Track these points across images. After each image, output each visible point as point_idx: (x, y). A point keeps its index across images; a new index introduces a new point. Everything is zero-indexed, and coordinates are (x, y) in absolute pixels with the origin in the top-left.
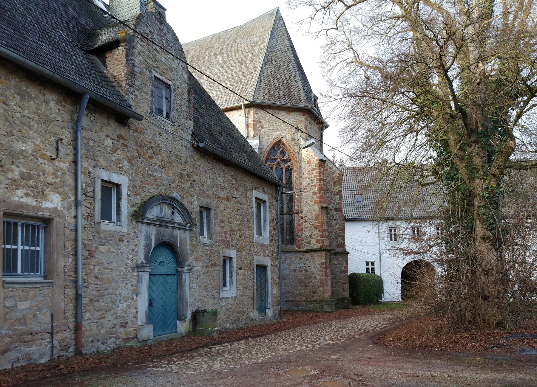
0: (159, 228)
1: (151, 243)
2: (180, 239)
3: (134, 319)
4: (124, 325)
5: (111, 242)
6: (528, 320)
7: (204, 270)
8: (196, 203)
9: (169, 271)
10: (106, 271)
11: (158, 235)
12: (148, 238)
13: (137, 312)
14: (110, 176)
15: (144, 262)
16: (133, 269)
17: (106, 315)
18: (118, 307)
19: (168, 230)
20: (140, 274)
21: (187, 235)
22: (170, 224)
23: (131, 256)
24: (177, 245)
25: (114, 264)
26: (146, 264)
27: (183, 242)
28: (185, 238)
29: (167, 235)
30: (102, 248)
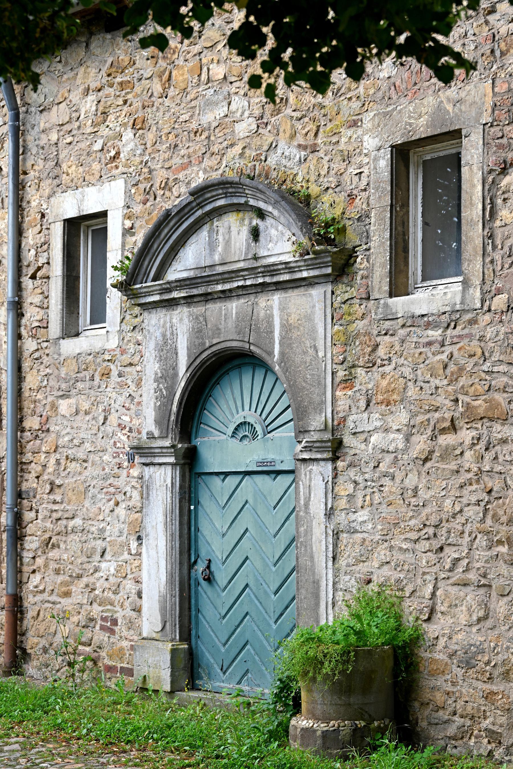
0: (198, 309)
1: (175, 368)
2: (287, 328)
3: (134, 614)
4: (110, 625)
5: (80, 385)
6: (247, 152)
7: (421, 444)
8: (370, 143)
9: (271, 456)
10: (73, 466)
11: (197, 333)
12: (167, 351)
13: (139, 595)
14: (82, 200)
15: (156, 434)
16: (131, 459)
17: (74, 589)
18: (96, 570)
19: (234, 306)
20: (148, 471)
21: (313, 303)
22: (225, 281)
23: (127, 419)
24: (271, 353)
25: (88, 446)
26: (161, 437)
27: (295, 334)
28: (309, 318)
29: (231, 324)
30: (65, 406)
